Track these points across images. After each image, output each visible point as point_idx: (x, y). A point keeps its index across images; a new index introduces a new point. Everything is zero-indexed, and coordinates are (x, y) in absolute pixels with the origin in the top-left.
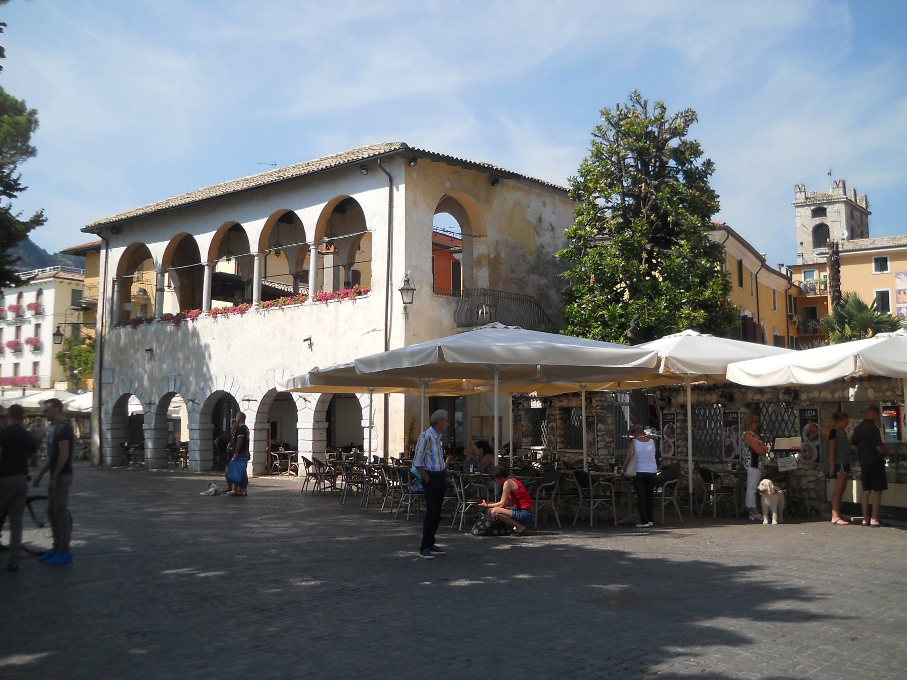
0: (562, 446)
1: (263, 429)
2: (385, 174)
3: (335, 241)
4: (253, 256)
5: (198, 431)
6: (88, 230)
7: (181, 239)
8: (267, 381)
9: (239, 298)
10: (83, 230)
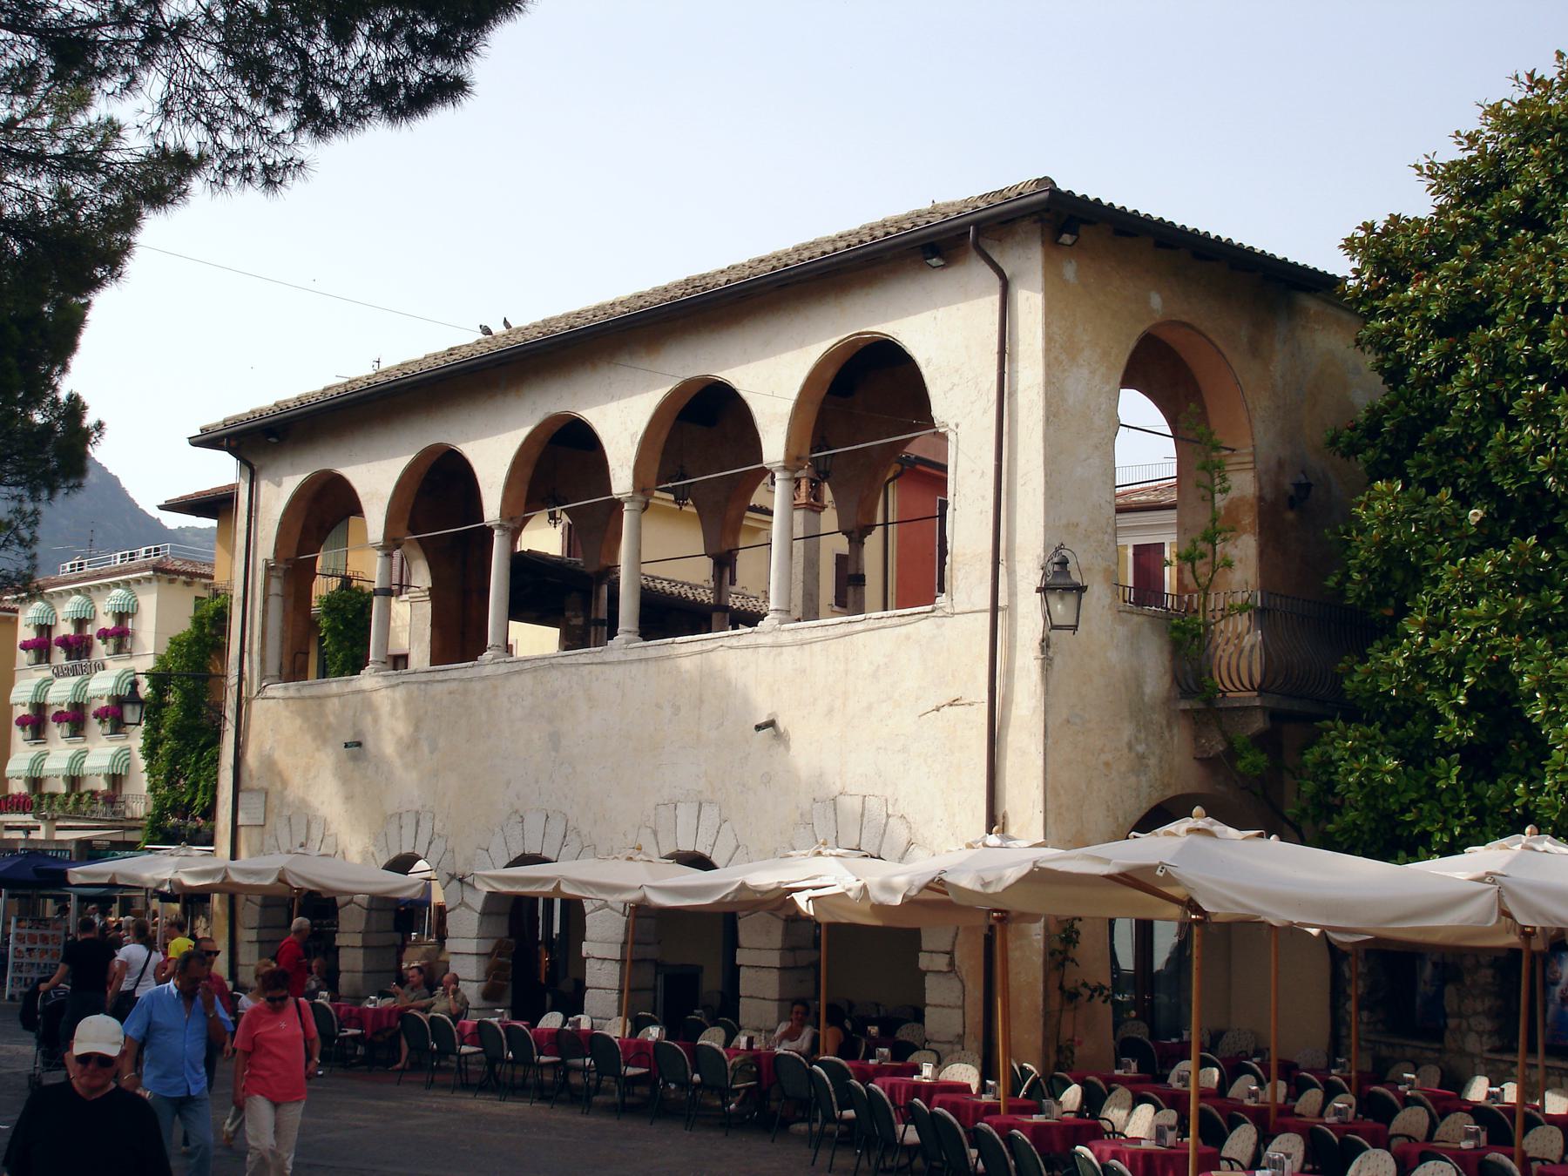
0: (1498, 1044)
1: (644, 960)
2: (988, 267)
3: (204, 842)
4: (617, 505)
5: (474, 958)
6: (209, 440)
7: (435, 458)
8: (655, 833)
9: (576, 616)
10: (196, 442)
